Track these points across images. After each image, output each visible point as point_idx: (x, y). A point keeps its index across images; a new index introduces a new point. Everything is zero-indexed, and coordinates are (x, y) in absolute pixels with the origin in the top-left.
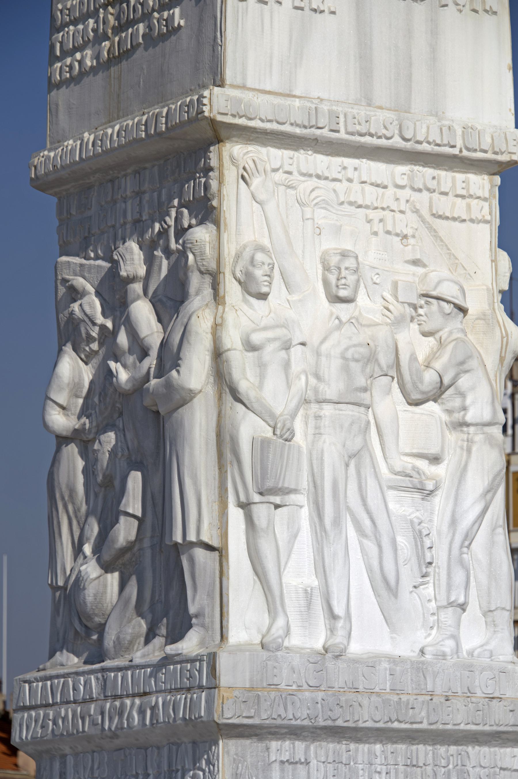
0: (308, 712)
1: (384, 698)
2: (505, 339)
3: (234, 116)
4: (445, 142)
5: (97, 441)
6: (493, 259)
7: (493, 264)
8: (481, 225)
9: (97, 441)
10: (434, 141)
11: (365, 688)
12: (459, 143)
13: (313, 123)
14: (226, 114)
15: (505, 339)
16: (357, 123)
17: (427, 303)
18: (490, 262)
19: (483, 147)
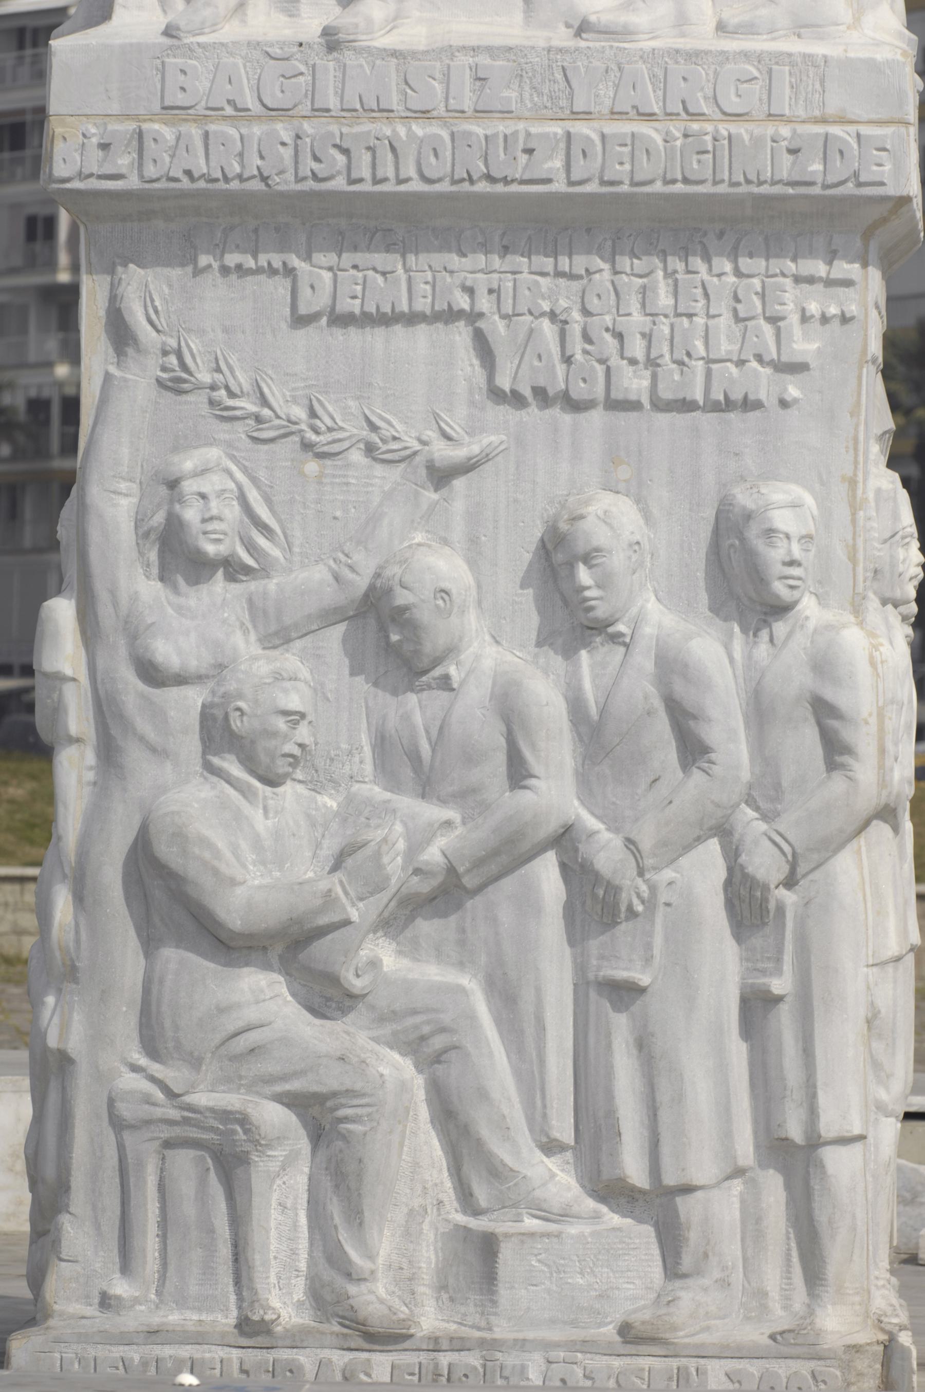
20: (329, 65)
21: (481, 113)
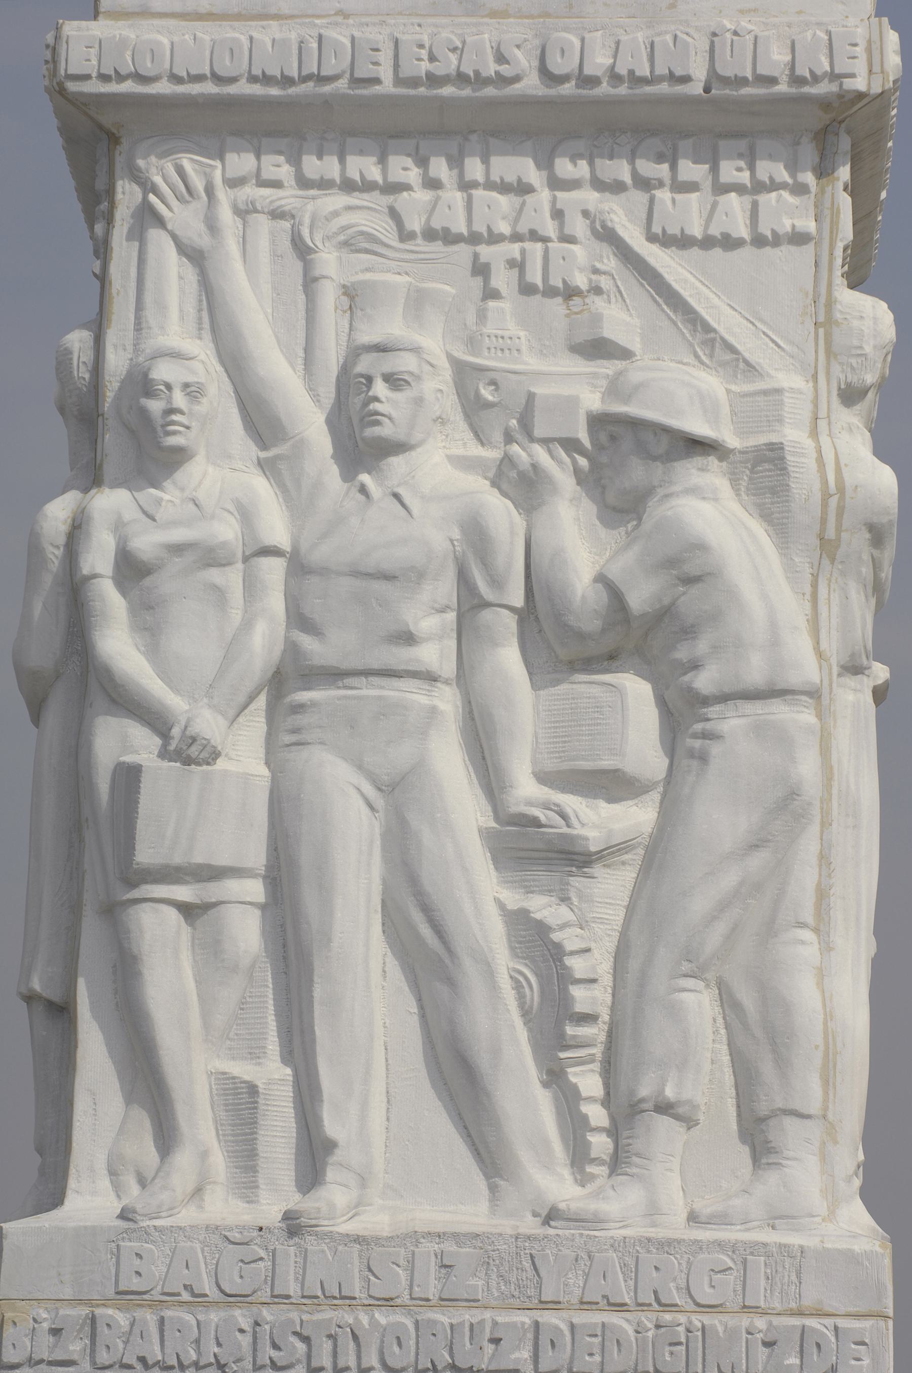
0: (216, 1350)
1: (419, 1318)
2: (833, 502)
3: (104, 78)
4: (661, 69)
5: (587, 443)
6: (821, 318)
7: (821, 331)
8: (785, 251)
9: (587, 443)
10: (631, 72)
11: (370, 1296)
12: (699, 73)
13: (312, 67)
14: (87, 77)
15: (833, 502)
16: (426, 57)
17: (613, 438)
18: (812, 329)
19: (762, 70)
20: (289, 1251)
21: (446, 1301)
